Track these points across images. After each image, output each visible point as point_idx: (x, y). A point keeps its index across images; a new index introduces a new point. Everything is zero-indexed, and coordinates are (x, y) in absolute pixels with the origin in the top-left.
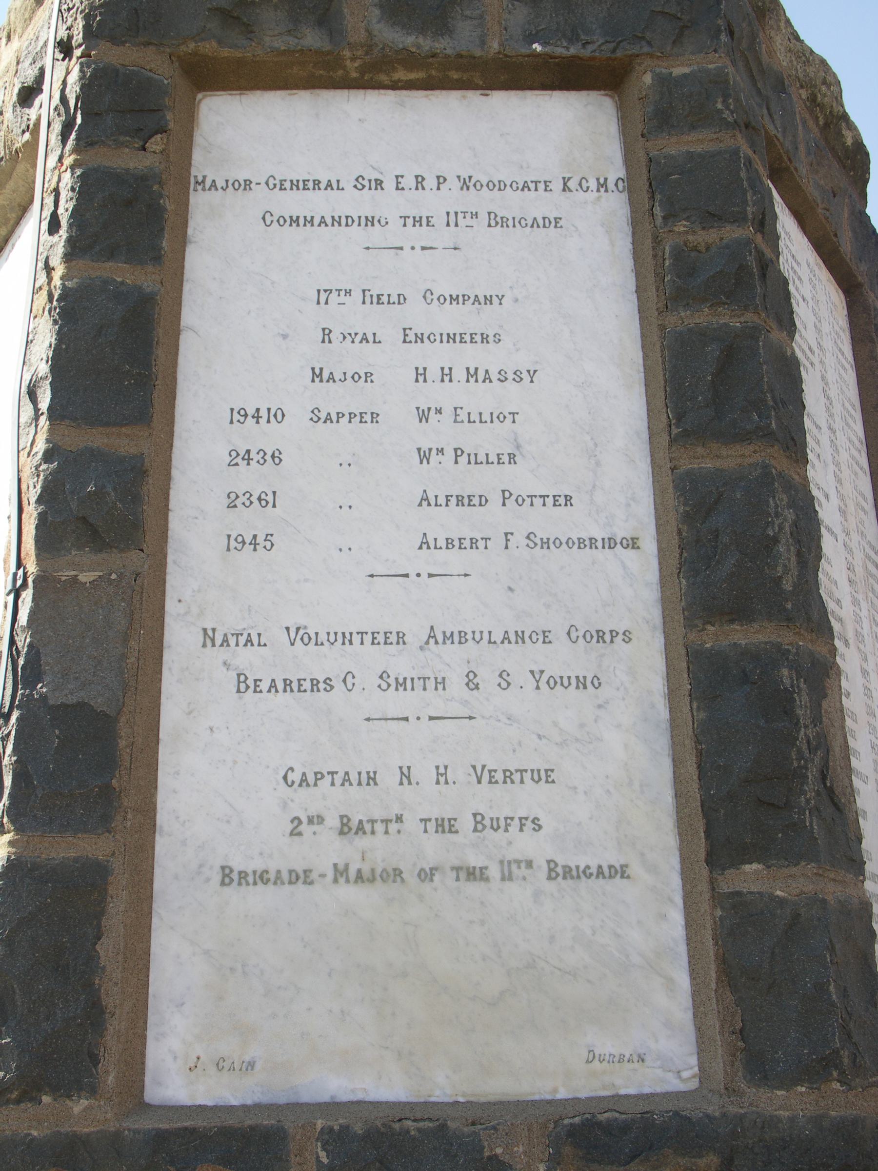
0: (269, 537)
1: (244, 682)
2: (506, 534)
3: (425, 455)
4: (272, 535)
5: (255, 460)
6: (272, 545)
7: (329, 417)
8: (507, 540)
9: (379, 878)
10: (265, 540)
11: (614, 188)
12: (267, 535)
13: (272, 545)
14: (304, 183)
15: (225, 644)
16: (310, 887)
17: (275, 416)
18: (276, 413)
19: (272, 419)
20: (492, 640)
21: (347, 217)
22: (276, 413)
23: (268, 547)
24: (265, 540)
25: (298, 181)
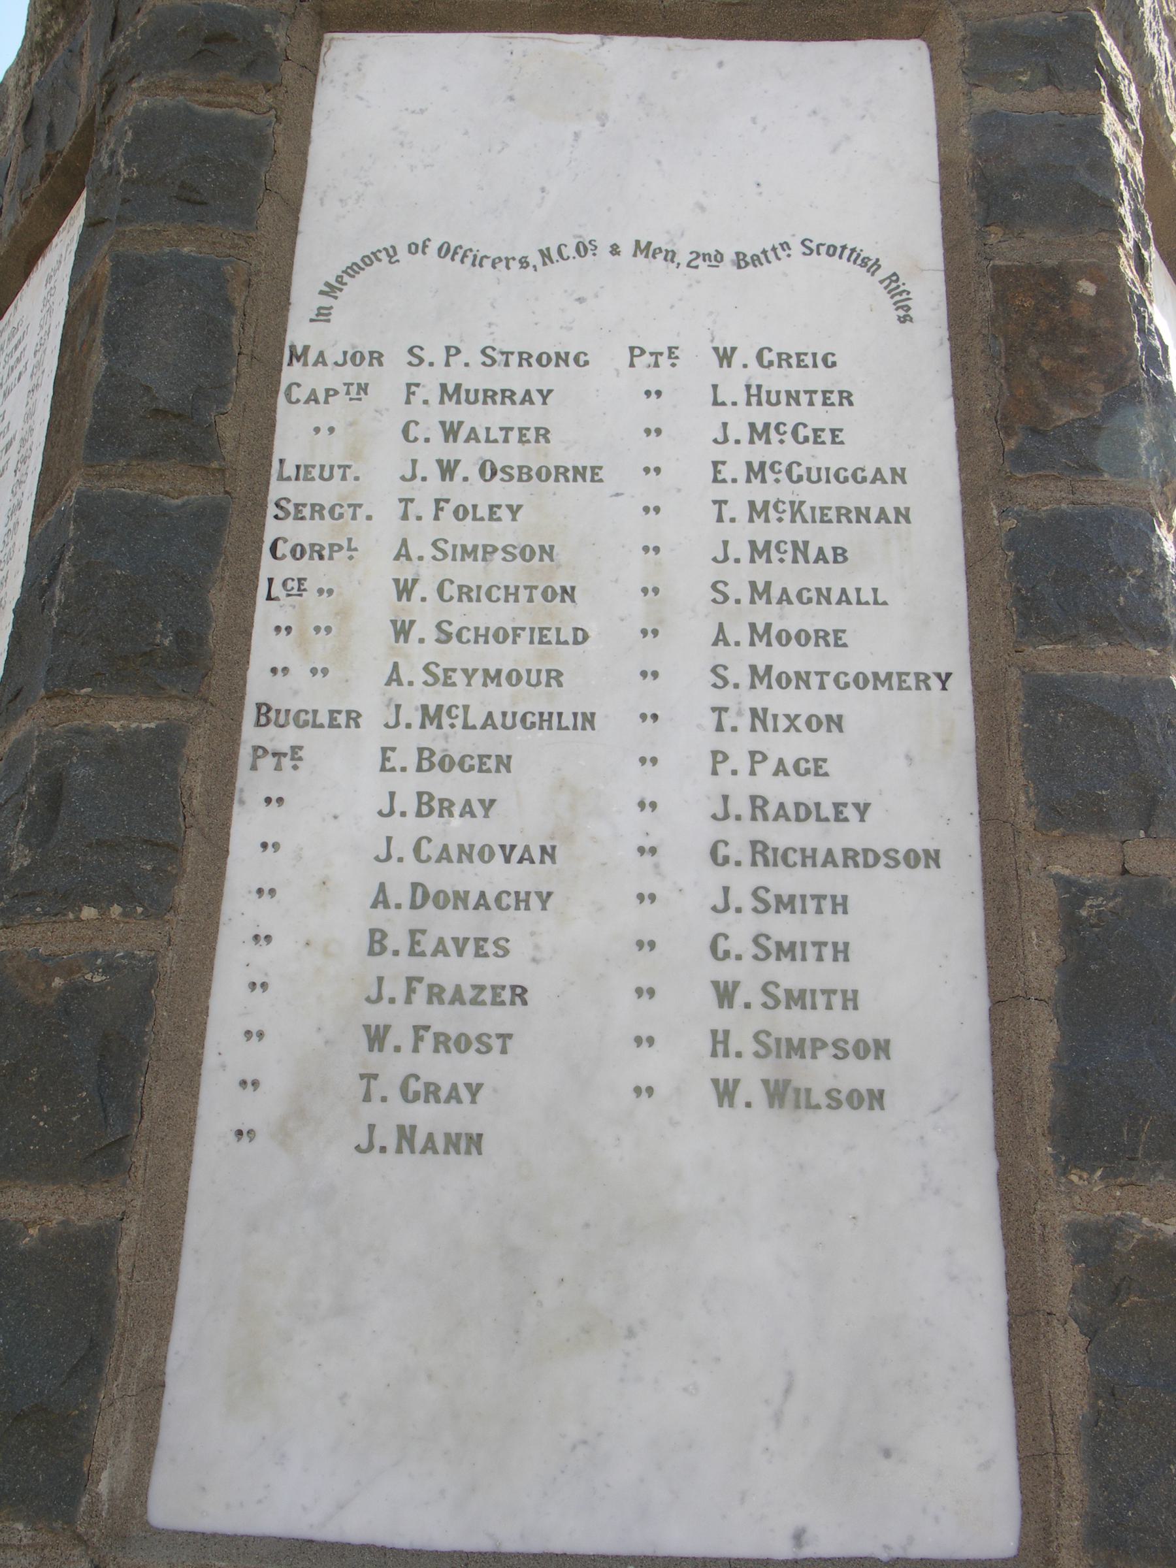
9: (291, 721)
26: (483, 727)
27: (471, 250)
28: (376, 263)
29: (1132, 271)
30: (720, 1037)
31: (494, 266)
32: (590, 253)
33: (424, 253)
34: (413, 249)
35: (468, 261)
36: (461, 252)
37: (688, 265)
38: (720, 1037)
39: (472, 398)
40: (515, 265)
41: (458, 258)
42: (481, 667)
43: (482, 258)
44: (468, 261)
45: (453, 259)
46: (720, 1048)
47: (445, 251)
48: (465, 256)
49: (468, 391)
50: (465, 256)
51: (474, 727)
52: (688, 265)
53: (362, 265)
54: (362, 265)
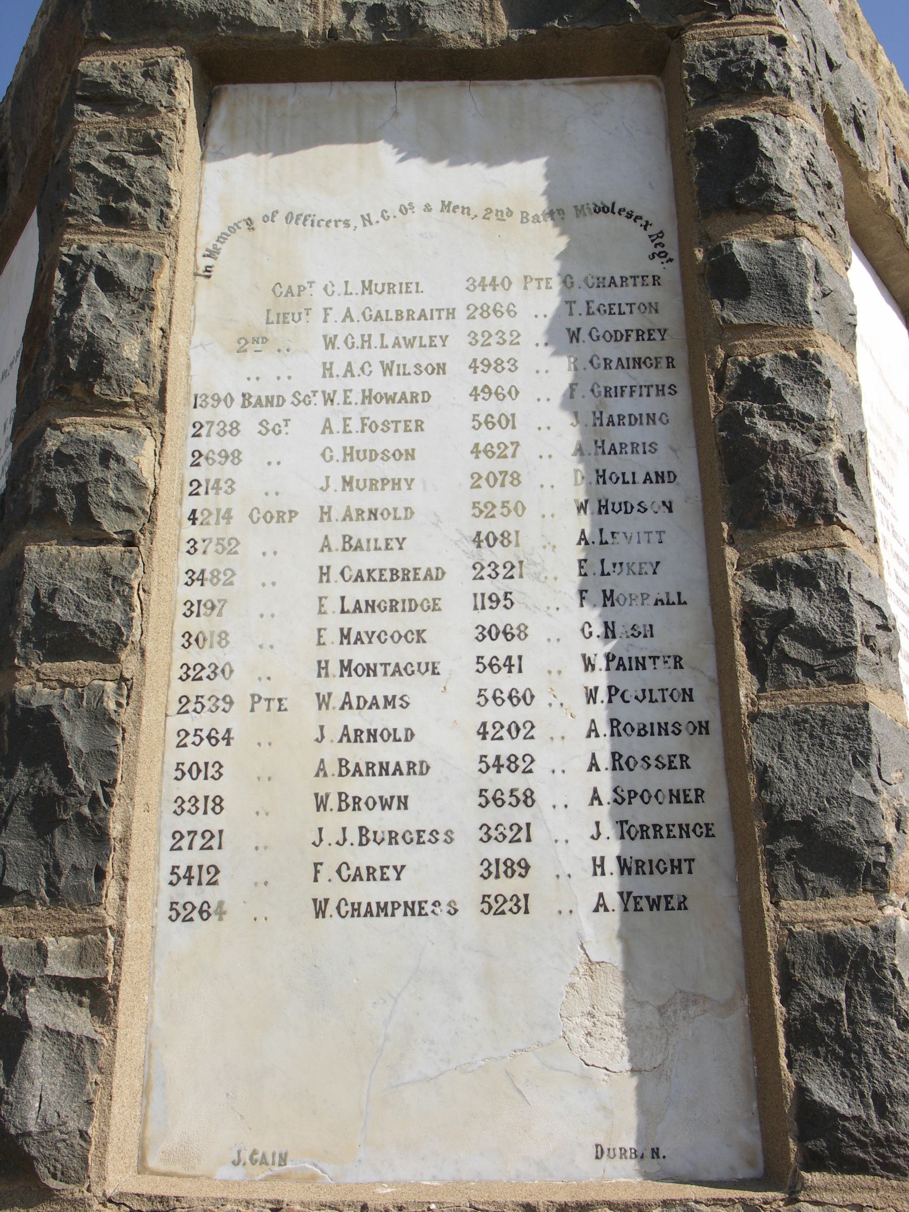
0: (484, 759)
1: (345, 766)
2: (316, 865)
3: (322, 801)
4: (485, 690)
5: (224, 489)
6: (512, 604)
7: (347, 700)
8: (317, 872)
9: (295, 217)
10: (177, 770)
11: (361, 318)
12: (484, 896)
13: (512, 604)
14: (382, 870)
15: (321, 774)
16: (252, 218)
17: (199, 771)
18: (198, 774)
19: (202, 767)
20: (322, 642)
21: (410, 600)
22: (198, 774)
23: (482, 703)
24: (177, 770)
25: (413, 903)
26: (354, 611)
27: (310, 216)
28: (238, 231)
29: (125, 235)
30: (598, 862)
31: (336, 226)
32: (409, 211)
33: (273, 221)
34: (265, 219)
35: (309, 223)
36: (302, 218)
37: (484, 218)
38: (598, 862)
39: (361, 485)
40: (341, 225)
41: (301, 222)
42: (390, 777)
43: (319, 222)
44: (309, 223)
45: (297, 223)
46: (599, 870)
47: (289, 218)
48: (305, 220)
49: (358, 481)
50: (305, 220)
51: (348, 612)
52: (484, 218)
53: (229, 233)
54: (229, 233)
